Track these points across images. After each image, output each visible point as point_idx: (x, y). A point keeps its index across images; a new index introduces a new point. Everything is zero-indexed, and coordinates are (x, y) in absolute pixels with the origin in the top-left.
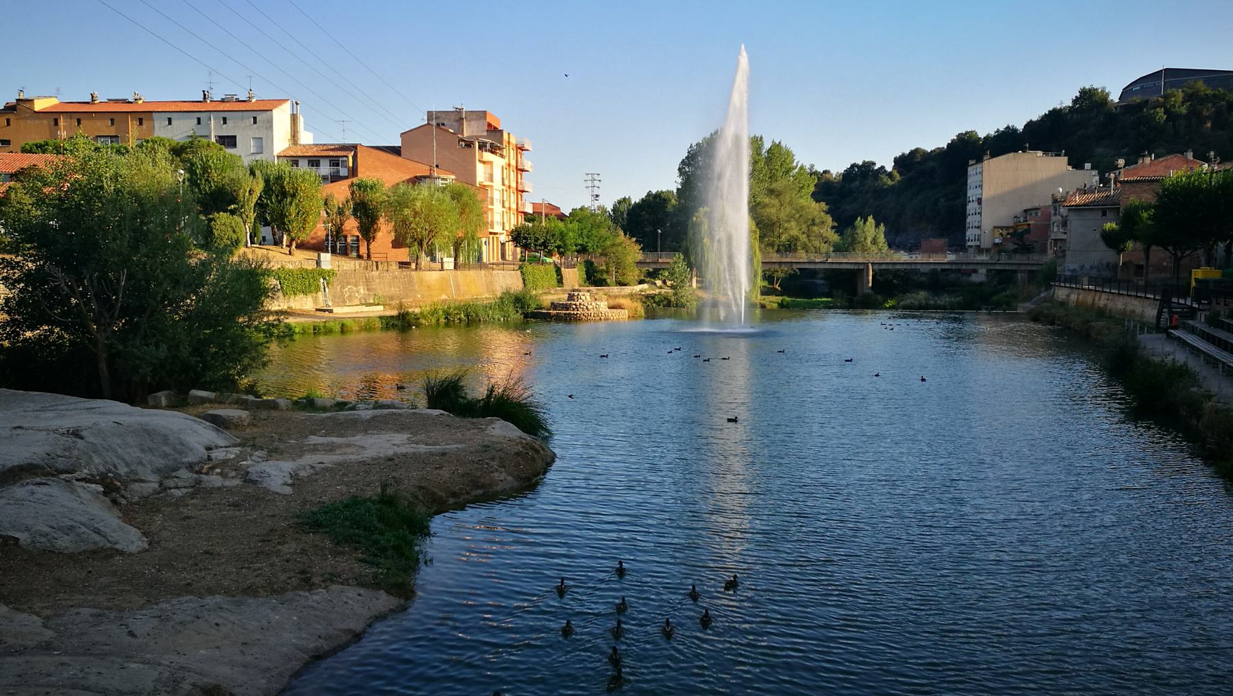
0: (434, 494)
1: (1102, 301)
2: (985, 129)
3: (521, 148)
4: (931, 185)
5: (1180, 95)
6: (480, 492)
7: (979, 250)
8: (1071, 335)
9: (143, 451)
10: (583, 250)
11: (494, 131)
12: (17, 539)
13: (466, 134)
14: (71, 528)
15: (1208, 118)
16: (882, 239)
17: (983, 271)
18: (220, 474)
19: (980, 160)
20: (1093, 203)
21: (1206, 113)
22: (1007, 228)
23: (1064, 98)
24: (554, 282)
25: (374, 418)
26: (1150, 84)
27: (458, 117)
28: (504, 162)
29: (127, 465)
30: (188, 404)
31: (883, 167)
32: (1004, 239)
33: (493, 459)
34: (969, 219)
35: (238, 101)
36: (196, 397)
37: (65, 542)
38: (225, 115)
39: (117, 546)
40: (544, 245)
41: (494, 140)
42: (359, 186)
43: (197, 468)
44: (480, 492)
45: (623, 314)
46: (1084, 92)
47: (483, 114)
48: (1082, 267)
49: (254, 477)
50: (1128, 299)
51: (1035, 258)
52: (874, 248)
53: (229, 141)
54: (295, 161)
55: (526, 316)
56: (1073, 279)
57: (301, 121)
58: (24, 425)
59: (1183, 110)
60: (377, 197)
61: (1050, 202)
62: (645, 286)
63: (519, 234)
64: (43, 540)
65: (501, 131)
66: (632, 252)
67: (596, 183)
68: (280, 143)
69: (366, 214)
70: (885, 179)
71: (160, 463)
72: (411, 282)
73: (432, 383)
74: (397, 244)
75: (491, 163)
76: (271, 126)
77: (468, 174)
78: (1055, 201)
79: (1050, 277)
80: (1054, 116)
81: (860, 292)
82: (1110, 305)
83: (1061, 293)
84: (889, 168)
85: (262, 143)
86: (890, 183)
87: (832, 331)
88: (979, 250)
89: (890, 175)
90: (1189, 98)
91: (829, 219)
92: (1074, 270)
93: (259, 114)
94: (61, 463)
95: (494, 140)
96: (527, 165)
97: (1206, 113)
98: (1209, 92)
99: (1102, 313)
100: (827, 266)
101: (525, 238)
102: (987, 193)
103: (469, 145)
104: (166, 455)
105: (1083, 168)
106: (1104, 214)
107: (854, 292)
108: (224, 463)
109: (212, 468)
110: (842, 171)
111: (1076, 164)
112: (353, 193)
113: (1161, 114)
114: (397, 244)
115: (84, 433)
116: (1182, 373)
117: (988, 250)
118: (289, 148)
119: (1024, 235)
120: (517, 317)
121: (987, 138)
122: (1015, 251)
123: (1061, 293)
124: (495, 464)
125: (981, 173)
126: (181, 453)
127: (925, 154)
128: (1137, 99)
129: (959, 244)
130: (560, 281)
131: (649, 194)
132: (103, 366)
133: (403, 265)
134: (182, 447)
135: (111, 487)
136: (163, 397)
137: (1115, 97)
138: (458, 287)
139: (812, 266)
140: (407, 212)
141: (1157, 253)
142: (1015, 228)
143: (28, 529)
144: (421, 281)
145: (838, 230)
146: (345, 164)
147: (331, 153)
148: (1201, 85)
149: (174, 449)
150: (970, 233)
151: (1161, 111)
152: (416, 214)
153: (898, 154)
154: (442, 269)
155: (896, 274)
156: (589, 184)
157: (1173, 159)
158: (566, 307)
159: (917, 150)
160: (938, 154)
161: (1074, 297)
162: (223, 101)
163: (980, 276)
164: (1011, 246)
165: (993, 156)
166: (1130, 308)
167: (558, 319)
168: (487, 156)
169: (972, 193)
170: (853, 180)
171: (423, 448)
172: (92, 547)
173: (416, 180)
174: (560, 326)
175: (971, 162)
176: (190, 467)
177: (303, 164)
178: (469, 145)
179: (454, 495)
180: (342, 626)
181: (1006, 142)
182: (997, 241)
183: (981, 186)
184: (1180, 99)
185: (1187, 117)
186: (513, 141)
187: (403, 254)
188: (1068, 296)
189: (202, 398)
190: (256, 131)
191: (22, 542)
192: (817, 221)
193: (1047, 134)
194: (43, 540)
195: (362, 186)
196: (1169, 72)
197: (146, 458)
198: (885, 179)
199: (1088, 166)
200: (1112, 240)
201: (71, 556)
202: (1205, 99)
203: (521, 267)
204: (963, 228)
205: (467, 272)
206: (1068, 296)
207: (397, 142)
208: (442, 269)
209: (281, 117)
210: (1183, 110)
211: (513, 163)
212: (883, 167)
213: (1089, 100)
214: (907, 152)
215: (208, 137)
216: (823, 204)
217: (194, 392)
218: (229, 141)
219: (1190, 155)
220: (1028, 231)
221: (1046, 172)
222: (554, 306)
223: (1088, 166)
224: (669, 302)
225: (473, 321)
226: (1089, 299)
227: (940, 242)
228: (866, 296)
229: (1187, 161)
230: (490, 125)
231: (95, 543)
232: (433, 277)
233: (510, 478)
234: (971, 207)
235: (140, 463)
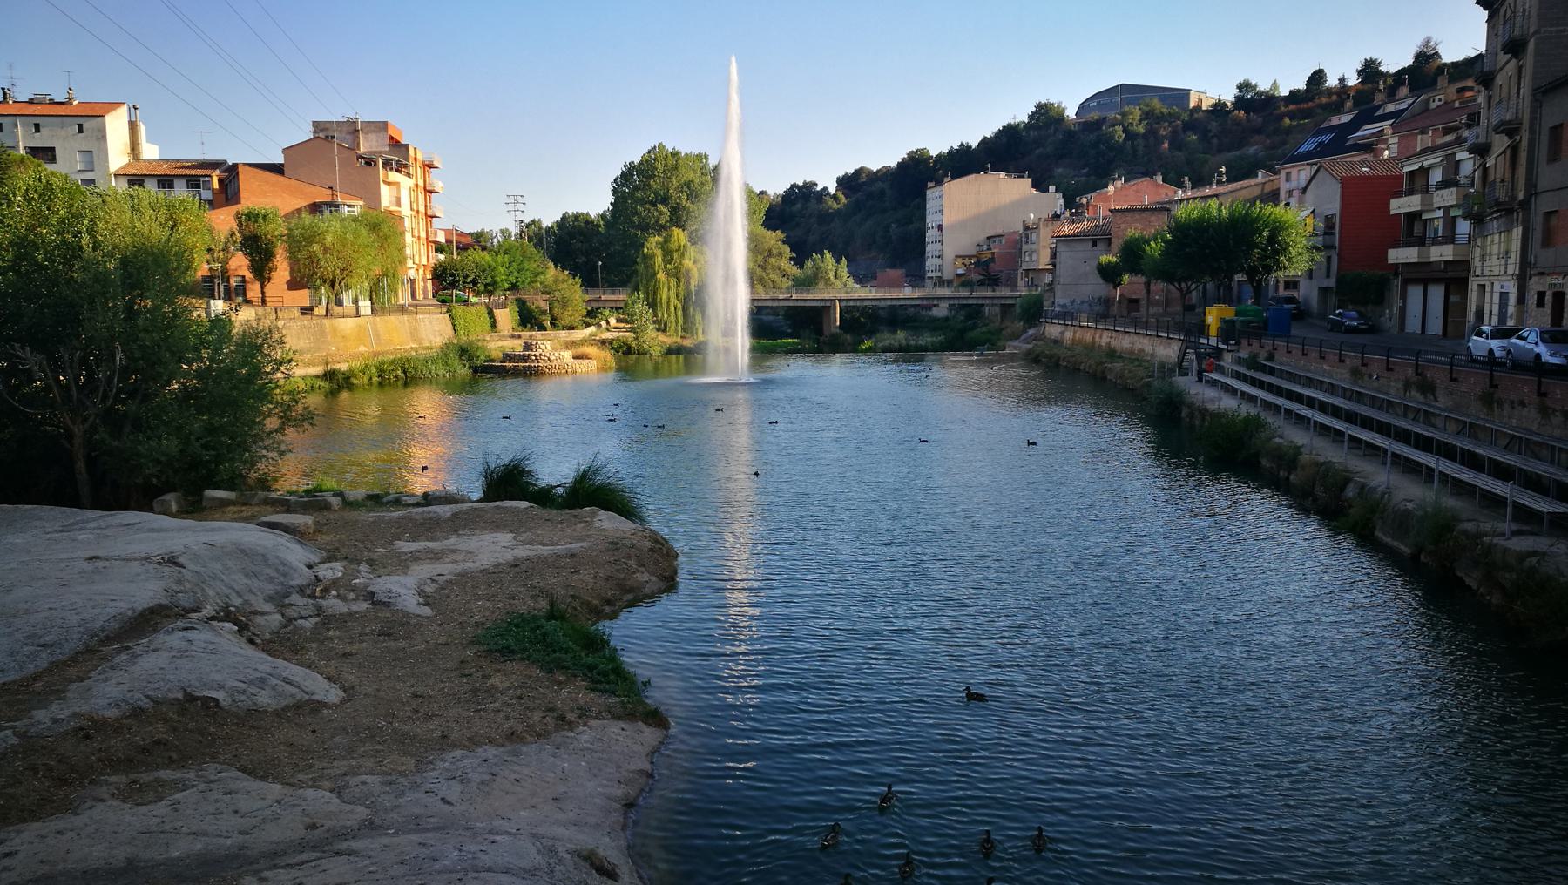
0: (588, 603)
1: (1104, 339)
2: (937, 146)
3: (429, 166)
4: (881, 211)
5: (1137, 113)
6: (630, 596)
7: (940, 282)
8: (1067, 377)
9: (247, 575)
10: (514, 287)
11: (396, 145)
12: (215, 700)
13: (362, 150)
14: (263, 680)
15: (1165, 137)
16: (844, 273)
17: (944, 305)
18: (338, 596)
19: (939, 182)
20: (1082, 233)
21: (1163, 133)
22: (970, 257)
23: (1021, 115)
24: (487, 326)
25: (455, 515)
26: (1107, 99)
27: (353, 128)
28: (411, 182)
29: (239, 595)
30: (202, 509)
31: (825, 189)
32: (968, 269)
33: (629, 557)
34: (929, 248)
35: (52, 102)
36: (214, 499)
37: (264, 699)
38: (37, 120)
39: (316, 697)
40: (474, 283)
41: (398, 156)
42: (249, 215)
43: (308, 592)
44: (630, 596)
45: (592, 365)
46: (1039, 107)
47: (383, 126)
48: (1073, 302)
49: (381, 597)
50: (1136, 338)
51: (1004, 292)
52: (838, 282)
53: (48, 154)
54: (136, 180)
55: (475, 370)
56: (1066, 315)
57: (142, 130)
58: (100, 554)
59: (1141, 129)
60: (276, 229)
61: (1020, 229)
62: (592, 329)
63: (444, 270)
64: (243, 698)
65: (407, 146)
66: (573, 291)
67: (520, 206)
68: (117, 157)
69: (259, 251)
70: (831, 202)
71: (270, 589)
72: (323, 332)
73: (492, 466)
74: (294, 285)
75: (397, 184)
76: (104, 137)
77: (373, 198)
78: (1027, 228)
79: (1034, 313)
80: (1009, 132)
81: (826, 333)
82: (1114, 343)
83: (1053, 330)
84: (832, 190)
85: (94, 155)
86: (835, 206)
87: (837, 378)
88: (940, 282)
89: (835, 197)
90: (1147, 115)
91: (787, 249)
92: (1064, 306)
93: (88, 120)
94: (184, 600)
95: (398, 156)
96: (438, 185)
97: (1163, 133)
98: (1165, 110)
99: (1112, 354)
100: (791, 304)
101: (452, 275)
102: (948, 219)
103: (370, 162)
104: (271, 580)
105: (1046, 190)
106: (1095, 245)
107: (819, 331)
108: (335, 583)
109: (326, 590)
110: (781, 191)
111: (1040, 185)
112: (240, 224)
113: (1119, 134)
114: (294, 285)
115: (181, 560)
116: (1254, 424)
117: (949, 283)
118: (128, 165)
119: (992, 264)
120: (463, 371)
121: (939, 156)
122: (981, 283)
123: (1053, 330)
124: (632, 562)
125: (941, 197)
126: (285, 575)
127: (870, 171)
128: (1095, 116)
129: (917, 276)
130: (494, 325)
131: (564, 218)
132: (81, 465)
133: (307, 311)
134: (284, 569)
135: (241, 621)
136: (172, 500)
137: (1071, 113)
138: (377, 335)
139: (775, 304)
140: (316, 247)
141: (1158, 286)
142: (978, 258)
143: (222, 687)
144: (334, 330)
145: (799, 262)
146: (208, 185)
147: (189, 172)
148: (1156, 103)
149: (277, 570)
150: (930, 263)
151: (1119, 129)
152: (326, 250)
153: (841, 174)
154: (358, 315)
155: (863, 311)
156: (511, 207)
157: (1143, 183)
158: (525, 359)
159: (862, 169)
160: (885, 174)
161: (1069, 335)
162: (31, 102)
163: (941, 311)
164: (976, 277)
165: (953, 178)
166: (1138, 346)
167: (516, 373)
168: (393, 176)
169: (931, 220)
170: (793, 202)
171: (544, 550)
172: (289, 701)
173: (315, 208)
174: (512, 383)
175: (930, 184)
176: (301, 590)
177: (151, 186)
178: (370, 162)
179: (609, 602)
180: (632, 767)
181: (963, 162)
182: (960, 271)
183: (941, 211)
184: (1138, 118)
185: (1144, 136)
186: (420, 157)
187: (303, 297)
188: (1062, 333)
189: (221, 500)
190: (81, 142)
191: (223, 704)
192: (775, 252)
193: (1004, 152)
194: (243, 698)
195: (252, 216)
196: (1125, 88)
197: (255, 584)
198: (831, 202)
199: (1052, 188)
200: (1109, 274)
201: (276, 714)
202: (1161, 118)
203: (449, 311)
204: (922, 253)
205: (387, 318)
206: (1062, 333)
207: (279, 159)
208: (358, 315)
209: (116, 126)
210: (1141, 129)
211: (421, 183)
212: (825, 189)
213: (1046, 116)
214: (851, 171)
215: (15, 148)
216: (779, 232)
217: (209, 493)
218: (48, 154)
219: (1159, 179)
220: (992, 260)
221: (1004, 197)
222: (507, 357)
223: (1052, 188)
224: (630, 347)
225: (413, 378)
226: (1088, 337)
227: (896, 273)
228: (833, 336)
229: (1158, 185)
230: (391, 138)
231: (292, 696)
232: (348, 325)
233: (654, 579)
234: (931, 235)
235: (250, 591)
